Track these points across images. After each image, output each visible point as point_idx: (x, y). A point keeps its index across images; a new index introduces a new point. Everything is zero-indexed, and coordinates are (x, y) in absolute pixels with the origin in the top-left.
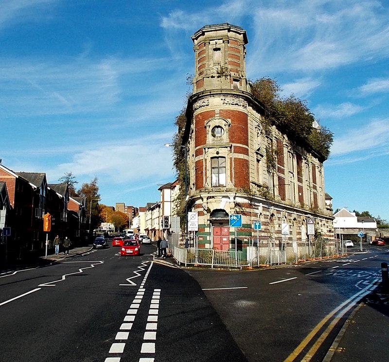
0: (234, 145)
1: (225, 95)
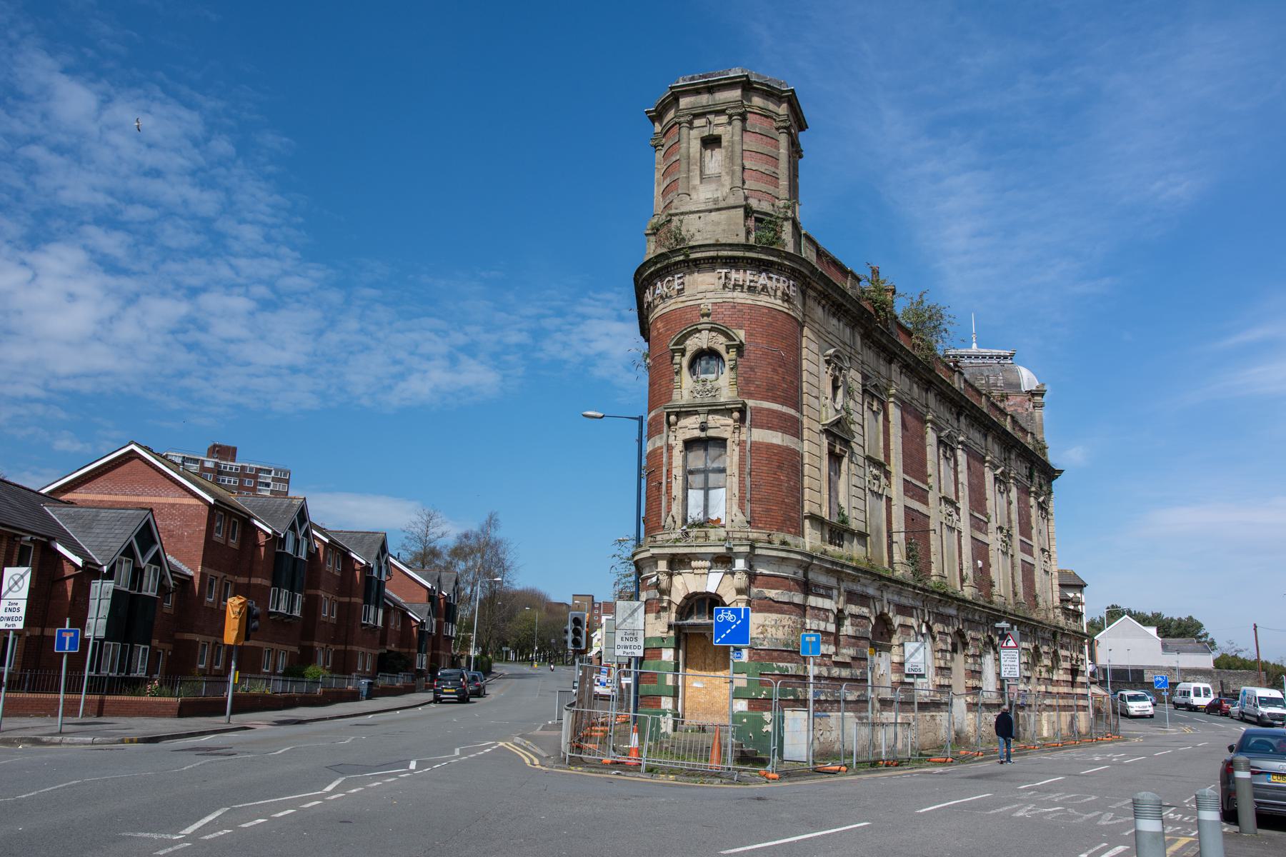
0: (751, 403)
1: (732, 263)
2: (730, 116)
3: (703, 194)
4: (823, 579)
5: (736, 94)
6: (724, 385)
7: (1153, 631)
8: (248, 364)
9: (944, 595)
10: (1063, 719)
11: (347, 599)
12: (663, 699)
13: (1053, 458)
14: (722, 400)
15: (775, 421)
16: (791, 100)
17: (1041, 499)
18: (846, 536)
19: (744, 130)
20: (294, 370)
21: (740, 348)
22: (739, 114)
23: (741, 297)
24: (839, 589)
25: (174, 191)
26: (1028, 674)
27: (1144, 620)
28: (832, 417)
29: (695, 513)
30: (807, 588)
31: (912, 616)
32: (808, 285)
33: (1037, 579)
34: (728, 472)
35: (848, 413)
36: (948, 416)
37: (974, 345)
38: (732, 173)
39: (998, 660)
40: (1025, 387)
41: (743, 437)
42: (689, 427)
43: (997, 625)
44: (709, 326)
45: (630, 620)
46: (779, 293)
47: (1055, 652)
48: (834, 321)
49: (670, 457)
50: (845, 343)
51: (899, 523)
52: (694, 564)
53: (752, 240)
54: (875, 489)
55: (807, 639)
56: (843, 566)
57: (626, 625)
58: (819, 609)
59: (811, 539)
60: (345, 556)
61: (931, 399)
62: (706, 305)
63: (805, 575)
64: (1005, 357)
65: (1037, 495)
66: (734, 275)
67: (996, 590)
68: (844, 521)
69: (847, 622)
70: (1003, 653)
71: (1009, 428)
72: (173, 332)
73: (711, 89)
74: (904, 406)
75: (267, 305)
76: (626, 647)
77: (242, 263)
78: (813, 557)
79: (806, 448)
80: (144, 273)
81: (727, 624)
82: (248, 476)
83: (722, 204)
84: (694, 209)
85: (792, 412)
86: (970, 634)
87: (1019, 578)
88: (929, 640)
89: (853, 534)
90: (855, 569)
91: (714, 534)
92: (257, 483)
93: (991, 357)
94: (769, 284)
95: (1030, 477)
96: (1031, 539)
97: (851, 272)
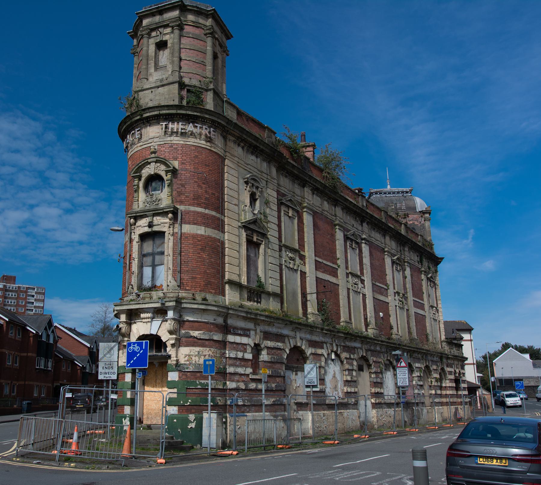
1: (170, 118)
2: (173, 27)
3: (155, 77)
4: (241, 324)
5: (176, 13)
6: (164, 197)
7: (527, 356)
8: (56, 241)
9: (348, 334)
11: (25, 354)
12: (125, 407)
13: (438, 251)
14: (162, 206)
15: (200, 219)
16: (214, 15)
17: (429, 276)
18: (263, 296)
19: (181, 36)
20: (81, 243)
21: (174, 172)
22: (178, 26)
23: (176, 140)
24: (256, 330)
25: (23, 160)
26: (421, 383)
27: (522, 350)
28: (249, 217)
29: (147, 282)
30: (226, 329)
32: (227, 132)
33: (428, 324)
34: (166, 253)
35: (266, 216)
36: (353, 222)
37: (389, 187)
38: (172, 62)
39: (395, 375)
40: (419, 209)
41: (176, 230)
42: (142, 226)
43: (394, 353)
44: (155, 159)
45: (108, 356)
46: (203, 137)
47: (443, 369)
48: (253, 157)
49: (131, 247)
50: (262, 172)
51: (311, 286)
52: (142, 315)
53: (184, 103)
54: (291, 266)
55: (207, 363)
56: (256, 314)
57: (105, 359)
58: (237, 344)
59: (231, 297)
60: (23, 328)
62: (154, 145)
63: (225, 321)
64: (407, 192)
65: (426, 273)
66: (170, 126)
67: (395, 330)
68: (261, 285)
69: (264, 352)
70: (398, 370)
71: (403, 232)
72: (20, 227)
73: (161, 12)
74: (315, 215)
75: (68, 211)
76: (106, 373)
77: (57, 192)
78: (228, 309)
79: (226, 238)
80: (8, 199)
81: (134, 353)
82: (22, 292)
83: (165, 82)
84: (148, 87)
85: (218, 215)
86: (372, 359)
87: (413, 324)
88: (338, 363)
89: (269, 294)
90: (267, 316)
91: (155, 295)
92: (27, 295)
93: (398, 193)
94: (195, 130)
95: (421, 261)
96: (423, 300)
97: (267, 127)
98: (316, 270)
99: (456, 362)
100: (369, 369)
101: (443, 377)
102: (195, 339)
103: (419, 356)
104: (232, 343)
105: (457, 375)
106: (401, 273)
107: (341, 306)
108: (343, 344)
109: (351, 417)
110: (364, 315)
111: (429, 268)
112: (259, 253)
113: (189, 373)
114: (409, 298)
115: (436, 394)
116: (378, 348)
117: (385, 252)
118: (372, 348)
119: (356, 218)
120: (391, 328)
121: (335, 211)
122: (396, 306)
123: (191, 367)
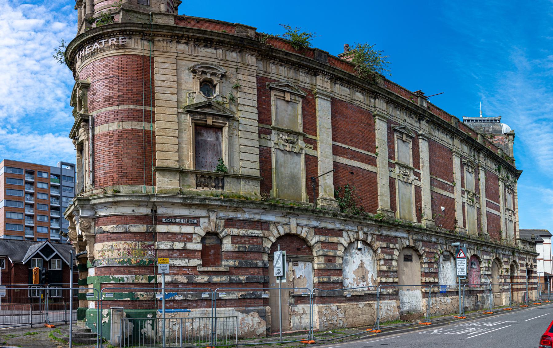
10: (519, 295)
13: (517, 166)
18: (226, 180)
26: (489, 273)
31: (342, 236)
40: (504, 131)
61: (457, 142)
64: (496, 120)
70: (458, 261)
72: (51, 152)
93: (488, 120)
96: (499, 203)
98: (334, 154)
99: (528, 257)
100: (420, 259)
101: (515, 268)
102: (109, 234)
103: (489, 249)
104: (165, 233)
105: (529, 267)
106: (473, 175)
107: (379, 194)
108: (377, 233)
109: (387, 308)
110: (417, 207)
111: (508, 177)
112: (222, 136)
113: (103, 269)
114: (481, 198)
115: (505, 282)
116: (434, 239)
117: (453, 152)
118: (425, 238)
119: (411, 115)
120: (456, 222)
121: (375, 103)
122: (464, 203)
123: (104, 263)
